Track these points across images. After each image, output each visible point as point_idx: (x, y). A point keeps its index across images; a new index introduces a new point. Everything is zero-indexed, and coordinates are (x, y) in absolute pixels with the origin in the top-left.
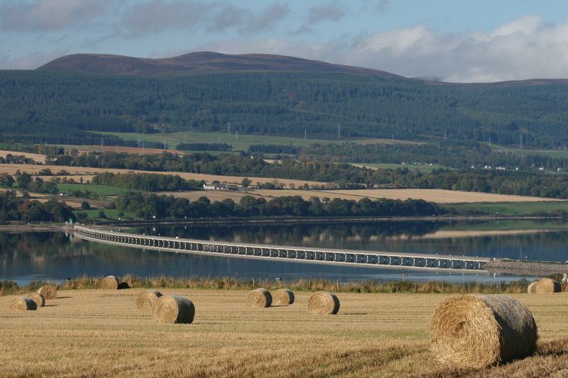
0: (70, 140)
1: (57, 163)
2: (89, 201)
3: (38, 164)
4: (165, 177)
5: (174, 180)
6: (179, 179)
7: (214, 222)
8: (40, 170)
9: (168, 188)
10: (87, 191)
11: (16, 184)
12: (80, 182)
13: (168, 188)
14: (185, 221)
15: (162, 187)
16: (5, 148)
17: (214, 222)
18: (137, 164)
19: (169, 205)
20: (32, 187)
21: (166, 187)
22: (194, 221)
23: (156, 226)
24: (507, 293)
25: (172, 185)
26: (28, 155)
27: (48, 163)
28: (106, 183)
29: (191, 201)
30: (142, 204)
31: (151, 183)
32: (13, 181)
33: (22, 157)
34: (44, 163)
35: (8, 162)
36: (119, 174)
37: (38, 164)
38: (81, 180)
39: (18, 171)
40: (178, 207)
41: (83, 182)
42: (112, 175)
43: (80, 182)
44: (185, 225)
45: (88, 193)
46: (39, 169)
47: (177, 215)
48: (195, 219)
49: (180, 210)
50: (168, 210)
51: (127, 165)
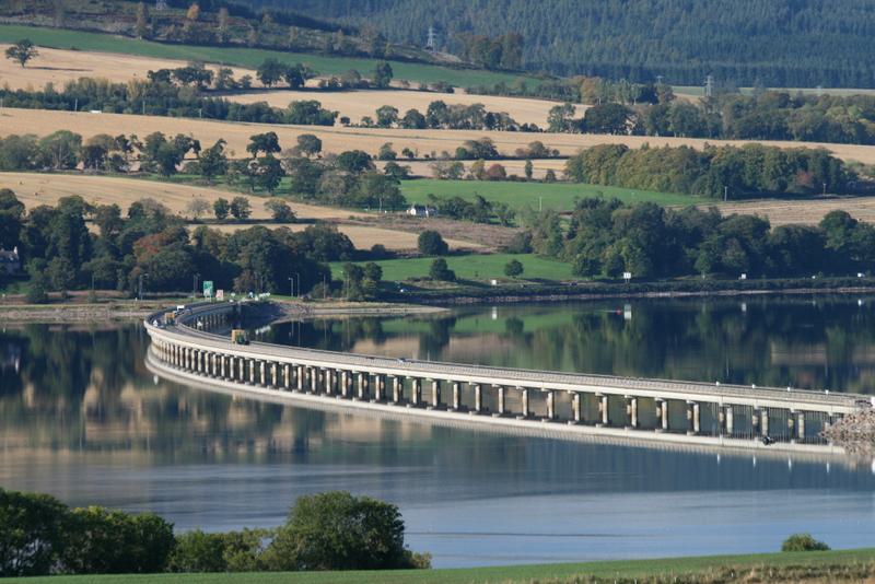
0: (859, 75)
1: (583, 126)
2: (564, 234)
3: (525, 129)
4: (782, 156)
5: (811, 166)
6: (826, 161)
7: (841, 290)
8: (461, 144)
9: (790, 188)
10: (482, 200)
11: (286, 182)
12: (524, 175)
13: (790, 188)
14: (739, 286)
15: (772, 186)
16: (531, 89)
17: (841, 290)
18: (825, 124)
19: (695, 237)
20: (326, 191)
21: (783, 186)
22: (771, 287)
23: (633, 301)
24: (304, 570)
25: (803, 179)
26: (494, 104)
27: (560, 125)
28: (603, 180)
29: (775, 223)
30: (605, 236)
31: (726, 172)
32: (283, 173)
33: (475, 110)
34: (546, 126)
35: (435, 124)
36: (645, 148)
37: (525, 129)
38: (529, 171)
39: (387, 146)
40: (724, 245)
41: (534, 176)
42: (623, 149)
43: (524, 175)
44: (739, 298)
45: (484, 203)
46: (525, 141)
47: (717, 267)
48: (777, 281)
49: (731, 255)
50: (689, 252)
51: (793, 127)
